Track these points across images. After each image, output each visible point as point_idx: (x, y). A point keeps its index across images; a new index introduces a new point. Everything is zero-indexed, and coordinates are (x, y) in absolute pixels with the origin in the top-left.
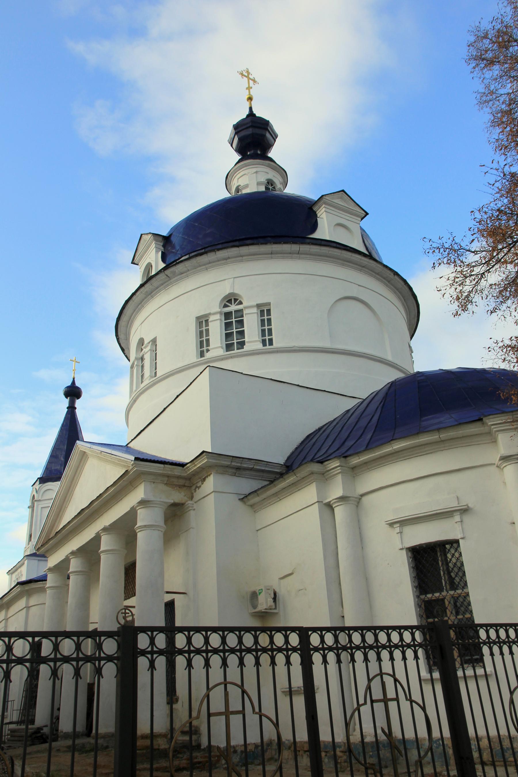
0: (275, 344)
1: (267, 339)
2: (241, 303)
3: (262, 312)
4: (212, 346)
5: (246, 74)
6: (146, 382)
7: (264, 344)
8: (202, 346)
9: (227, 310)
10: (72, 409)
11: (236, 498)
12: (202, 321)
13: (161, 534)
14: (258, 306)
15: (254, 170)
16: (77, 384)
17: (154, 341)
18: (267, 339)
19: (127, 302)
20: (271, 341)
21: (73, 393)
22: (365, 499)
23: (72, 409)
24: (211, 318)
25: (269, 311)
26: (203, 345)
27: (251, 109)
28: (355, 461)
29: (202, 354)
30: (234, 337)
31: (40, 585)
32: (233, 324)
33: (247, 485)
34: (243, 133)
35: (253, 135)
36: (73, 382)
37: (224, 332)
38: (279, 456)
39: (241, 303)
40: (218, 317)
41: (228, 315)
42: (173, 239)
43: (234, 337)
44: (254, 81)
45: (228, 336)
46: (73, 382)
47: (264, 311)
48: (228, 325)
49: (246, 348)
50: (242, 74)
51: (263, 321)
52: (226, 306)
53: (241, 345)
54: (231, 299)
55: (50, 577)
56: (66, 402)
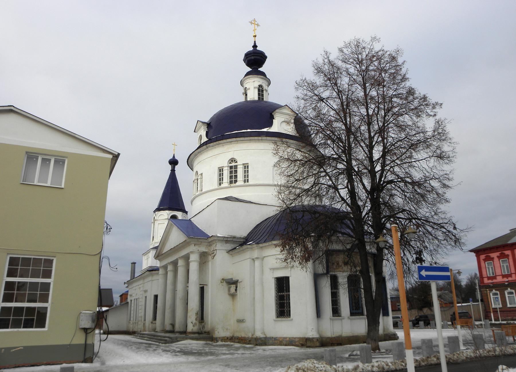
0: (250, 182)
1: (246, 180)
2: (236, 162)
3: (245, 167)
4: (224, 181)
5: (253, 22)
6: (198, 193)
7: (245, 182)
8: (220, 181)
9: (231, 165)
10: (173, 170)
11: (225, 251)
12: (221, 170)
13: (198, 264)
14: (243, 164)
15: (253, 80)
16: (176, 158)
17: (202, 174)
18: (246, 180)
19: (191, 154)
20: (248, 180)
21: (174, 162)
22: (265, 259)
23: (173, 170)
24: (238, 167)
25: (248, 166)
26: (221, 180)
27: (255, 42)
28: (261, 245)
29: (220, 185)
30: (233, 179)
31: (157, 272)
32: (233, 170)
33: (230, 246)
34: (249, 59)
35: (254, 59)
36: (174, 156)
37: (229, 175)
38: (244, 233)
39: (236, 162)
40: (226, 168)
41: (231, 167)
42: (211, 124)
43: (233, 179)
44: (258, 25)
45: (231, 177)
46: (174, 156)
47: (246, 167)
48: (231, 172)
49: (237, 184)
50: (251, 23)
51: (245, 171)
52: (230, 163)
53: (236, 181)
54: (233, 160)
55: (160, 270)
56: (170, 167)
